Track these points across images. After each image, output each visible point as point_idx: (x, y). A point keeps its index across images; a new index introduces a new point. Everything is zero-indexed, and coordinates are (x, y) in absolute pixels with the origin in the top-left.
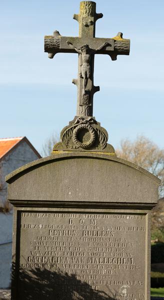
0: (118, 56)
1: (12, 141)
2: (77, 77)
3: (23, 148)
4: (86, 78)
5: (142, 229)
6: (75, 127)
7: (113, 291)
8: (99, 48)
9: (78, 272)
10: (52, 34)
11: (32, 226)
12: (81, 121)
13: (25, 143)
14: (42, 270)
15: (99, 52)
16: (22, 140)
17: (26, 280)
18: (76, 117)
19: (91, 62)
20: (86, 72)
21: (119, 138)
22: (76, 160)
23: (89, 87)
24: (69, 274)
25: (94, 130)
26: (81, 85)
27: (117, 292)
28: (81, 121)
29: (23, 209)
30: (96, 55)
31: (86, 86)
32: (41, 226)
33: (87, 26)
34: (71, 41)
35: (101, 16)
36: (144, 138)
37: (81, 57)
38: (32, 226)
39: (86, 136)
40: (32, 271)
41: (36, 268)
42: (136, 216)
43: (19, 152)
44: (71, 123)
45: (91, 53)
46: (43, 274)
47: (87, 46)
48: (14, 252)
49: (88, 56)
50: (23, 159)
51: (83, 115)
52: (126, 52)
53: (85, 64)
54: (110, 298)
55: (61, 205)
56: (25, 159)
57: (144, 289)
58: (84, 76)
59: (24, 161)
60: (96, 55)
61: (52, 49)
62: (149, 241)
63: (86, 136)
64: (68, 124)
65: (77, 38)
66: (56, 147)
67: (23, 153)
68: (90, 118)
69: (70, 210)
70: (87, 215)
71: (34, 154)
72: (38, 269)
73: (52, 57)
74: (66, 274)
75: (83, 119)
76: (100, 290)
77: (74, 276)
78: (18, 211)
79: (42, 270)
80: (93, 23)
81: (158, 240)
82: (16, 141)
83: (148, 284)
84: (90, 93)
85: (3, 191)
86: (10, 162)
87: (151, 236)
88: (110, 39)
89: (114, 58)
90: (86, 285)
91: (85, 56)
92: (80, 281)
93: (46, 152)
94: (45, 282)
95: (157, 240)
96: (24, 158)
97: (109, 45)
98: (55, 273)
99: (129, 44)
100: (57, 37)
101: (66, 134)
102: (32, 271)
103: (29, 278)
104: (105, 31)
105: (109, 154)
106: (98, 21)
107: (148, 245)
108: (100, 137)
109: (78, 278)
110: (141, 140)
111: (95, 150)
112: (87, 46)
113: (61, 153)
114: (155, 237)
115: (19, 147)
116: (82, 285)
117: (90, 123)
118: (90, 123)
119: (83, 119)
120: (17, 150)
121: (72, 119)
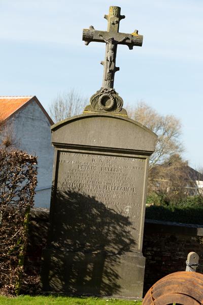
0: (134, 47)
1: (22, 99)
2: (104, 60)
3: (33, 107)
4: (111, 61)
5: (143, 168)
6: (101, 95)
7: (120, 209)
8: (121, 41)
9: (97, 195)
10: (88, 28)
11: (67, 162)
12: (105, 91)
13: (34, 103)
14: (72, 192)
15: (121, 43)
16: (31, 99)
17: (61, 198)
18: (102, 88)
19: (114, 50)
20: (111, 57)
21: (131, 101)
22: (100, 118)
23: (112, 68)
24: (91, 197)
25: (114, 98)
26: (107, 66)
27: (122, 210)
28: (105, 91)
29: (62, 149)
30: (118, 45)
31: (110, 66)
32: (73, 162)
33: (113, 24)
34: (102, 34)
35: (124, 17)
36: (144, 104)
37: (108, 46)
38: (67, 162)
39: (108, 102)
40: (65, 192)
41: (68, 191)
42: (139, 160)
43: (29, 110)
44: (98, 92)
45: (115, 43)
46: (73, 195)
47: (113, 39)
48: (53, 178)
49: (113, 45)
50: (32, 117)
51: (106, 87)
52: (140, 44)
53: (110, 51)
54: (117, 214)
55: (87, 148)
56: (34, 118)
57: (141, 209)
58: (109, 60)
59: (33, 119)
60: (118, 45)
61: (88, 39)
62: (144, 205)
63: (108, 102)
64: (95, 93)
65: (106, 32)
66: (86, 108)
67: (32, 111)
68: (111, 89)
69: (94, 152)
70: (105, 157)
71: (42, 112)
72: (70, 192)
73: (87, 44)
74: (89, 196)
75: (107, 90)
76: (111, 208)
77: (94, 198)
78: (58, 151)
79: (72, 192)
80: (118, 22)
81: (154, 204)
82: (26, 100)
83: (143, 217)
84: (112, 73)
85: (13, 146)
86: (19, 119)
87: (148, 198)
88: (129, 35)
89: (131, 48)
90: (102, 204)
91: (111, 45)
92: (98, 202)
93: (52, 111)
94: (74, 201)
95: (153, 204)
96: (33, 116)
97: (128, 39)
98: (80, 195)
99: (142, 39)
100: (92, 31)
101: (94, 99)
102: (65, 192)
103: (63, 197)
104: (126, 28)
105: (123, 115)
106: (122, 21)
107: (147, 169)
108: (117, 103)
109: (96, 199)
110: (141, 106)
111: (114, 112)
112: (113, 39)
113: (90, 113)
114: (151, 201)
115: (29, 106)
116: (99, 204)
117: (112, 93)
118: (112, 93)
119: (107, 90)
120: (27, 109)
121: (99, 89)
